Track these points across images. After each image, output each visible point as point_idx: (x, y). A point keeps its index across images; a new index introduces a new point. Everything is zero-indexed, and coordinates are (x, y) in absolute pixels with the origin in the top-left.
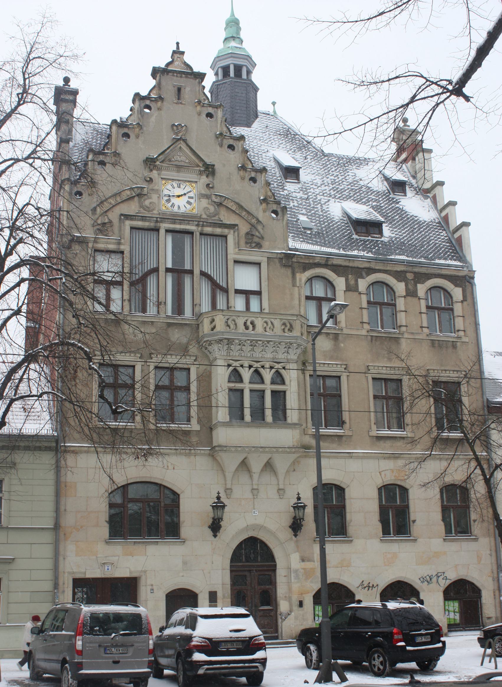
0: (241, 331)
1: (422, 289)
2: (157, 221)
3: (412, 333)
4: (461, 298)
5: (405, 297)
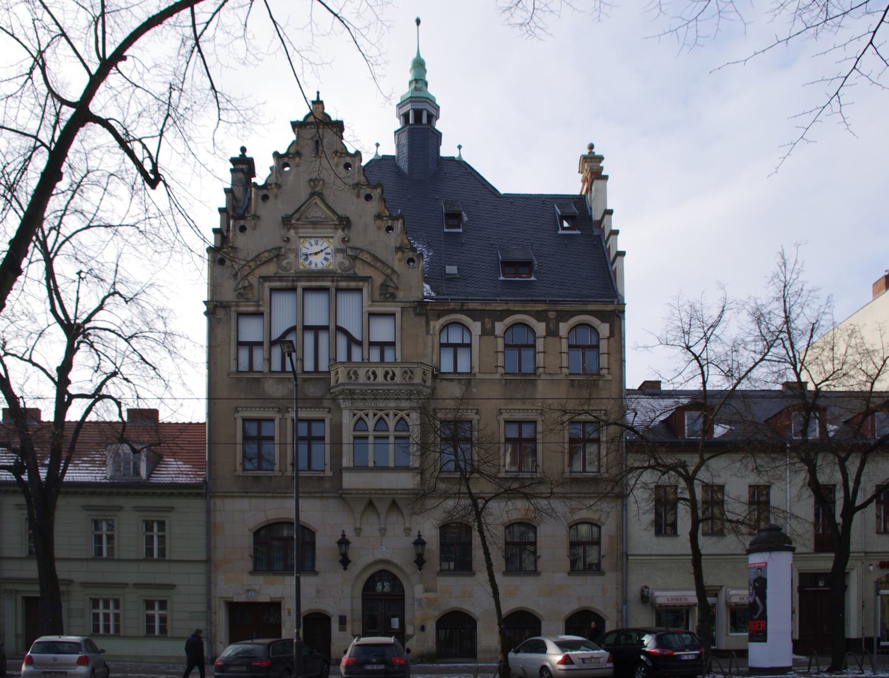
0: (361, 381)
1: (564, 328)
2: (293, 281)
3: (550, 374)
4: (607, 334)
5: (544, 337)
